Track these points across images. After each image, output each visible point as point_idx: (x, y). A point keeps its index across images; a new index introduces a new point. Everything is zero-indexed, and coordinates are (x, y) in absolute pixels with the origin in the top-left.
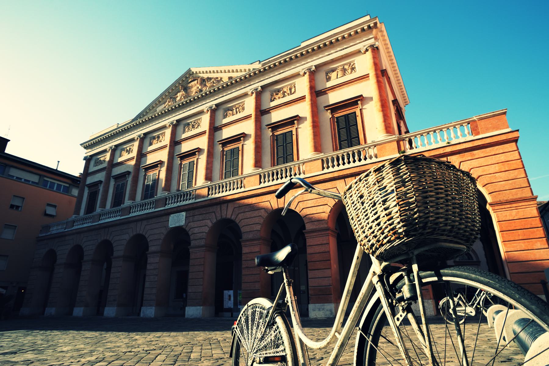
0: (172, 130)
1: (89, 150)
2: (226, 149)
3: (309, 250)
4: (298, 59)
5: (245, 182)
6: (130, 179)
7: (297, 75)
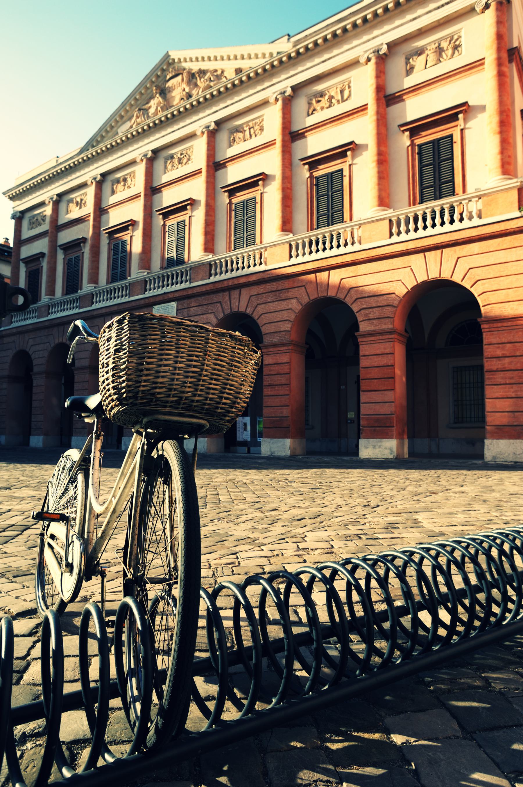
0: (147, 168)
1: (18, 202)
2: (235, 201)
3: (364, 362)
4: (358, 30)
5: (265, 255)
6: (87, 250)
7: (354, 64)
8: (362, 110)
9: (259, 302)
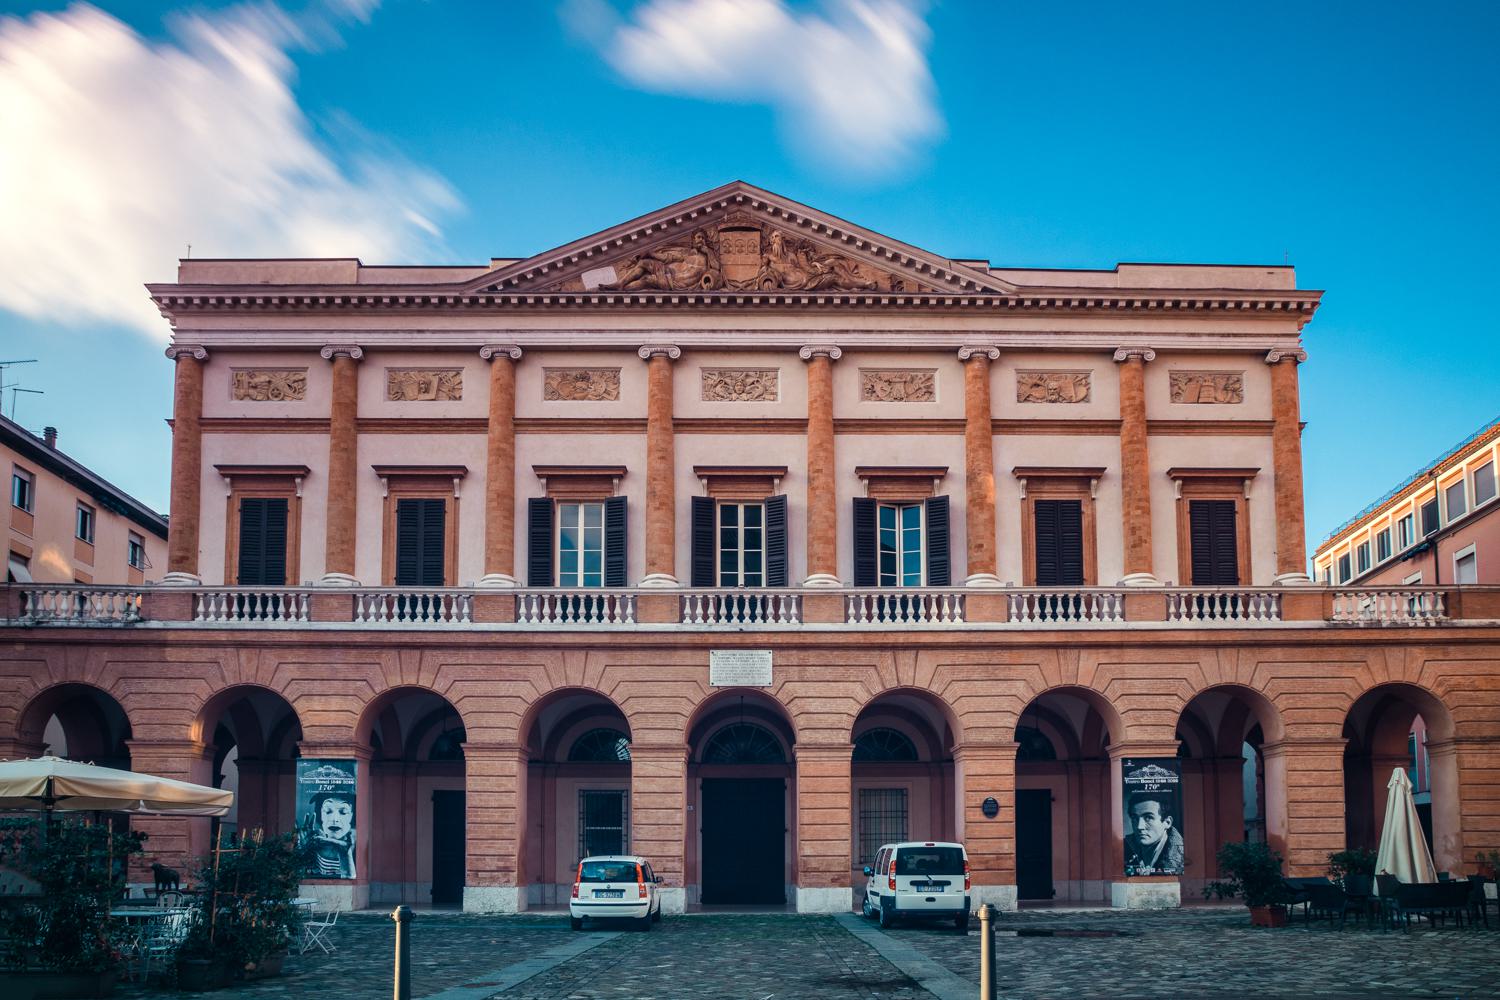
8: (959, 426)
9: (955, 677)
